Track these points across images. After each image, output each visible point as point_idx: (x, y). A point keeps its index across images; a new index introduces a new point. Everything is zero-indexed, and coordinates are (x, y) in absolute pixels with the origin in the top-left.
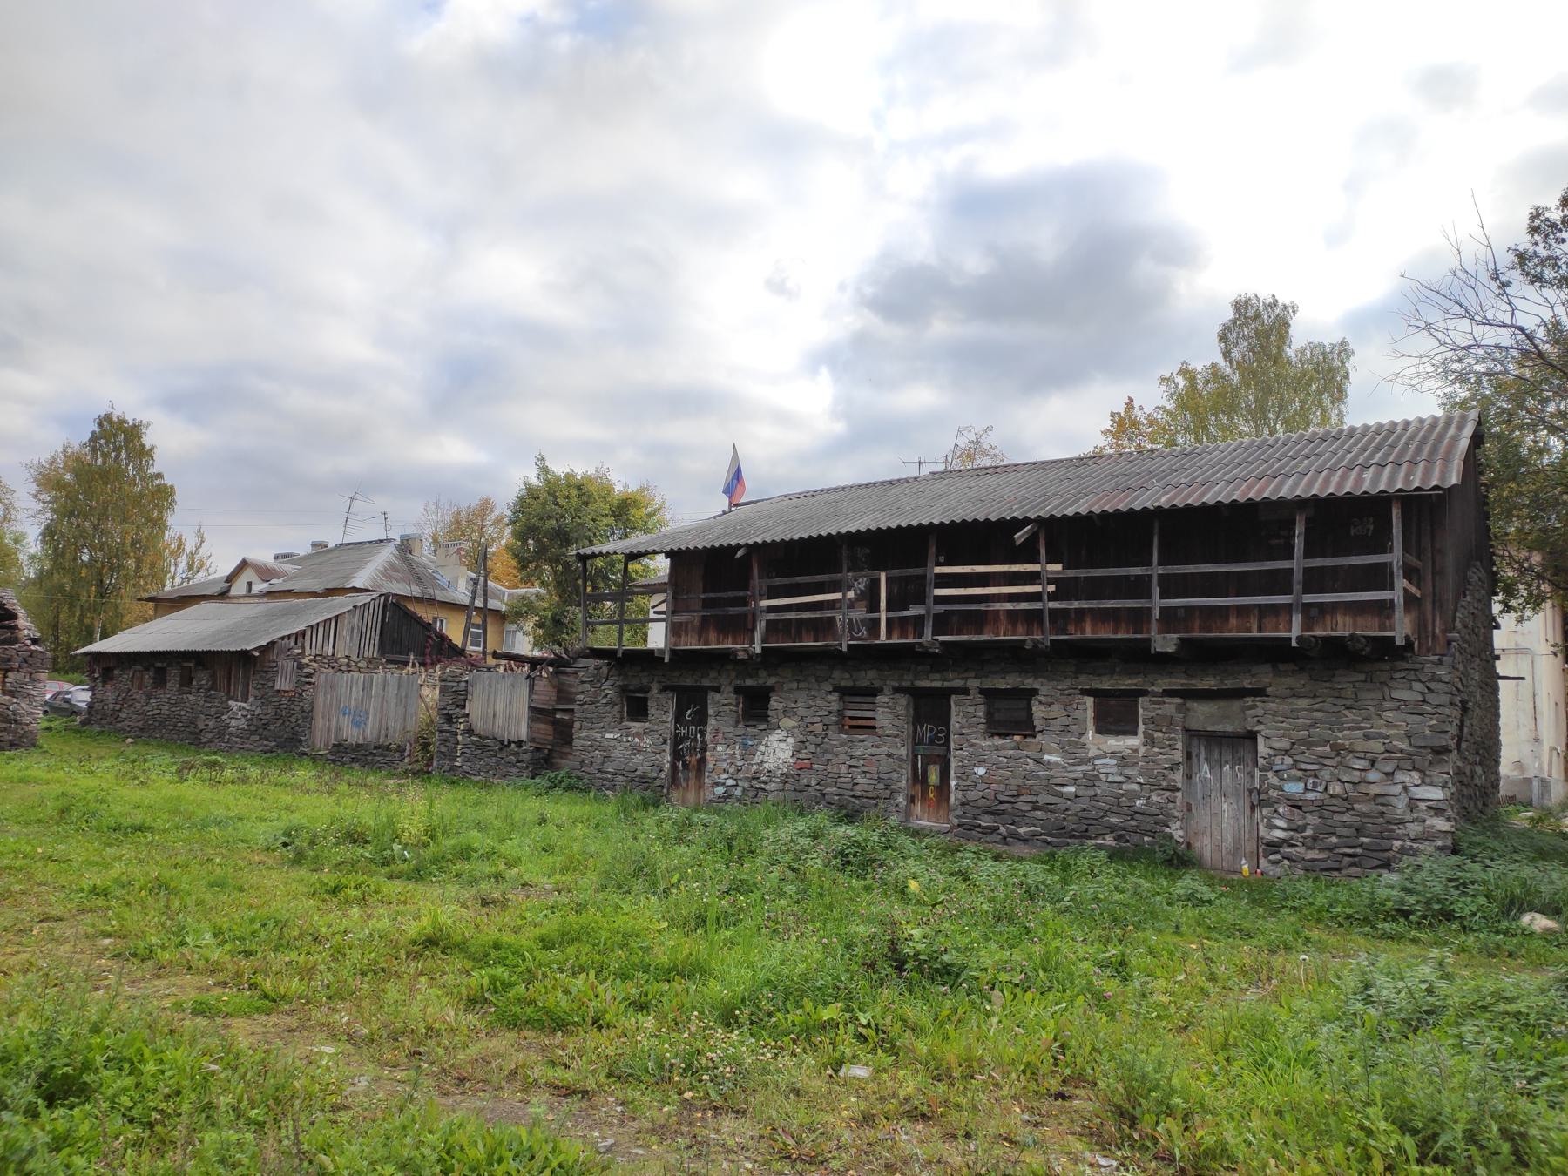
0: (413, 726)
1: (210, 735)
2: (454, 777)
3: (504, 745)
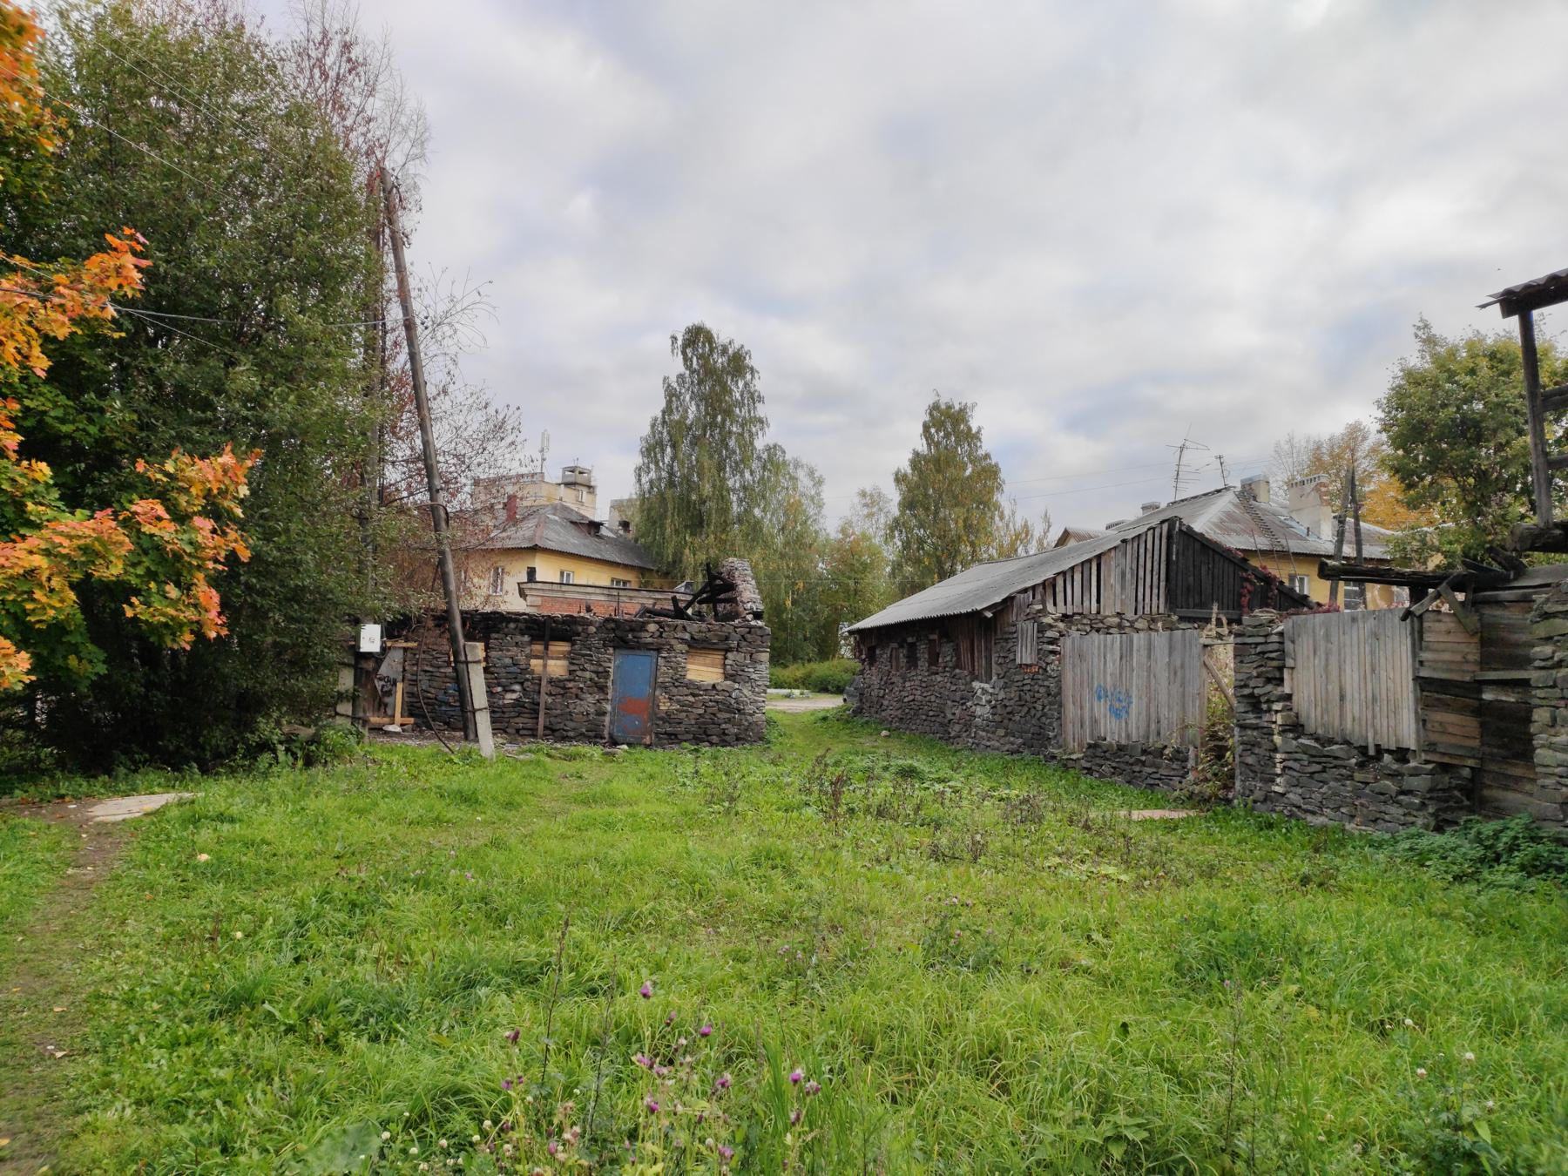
0: (1196, 717)
1: (957, 728)
2: (1269, 817)
3: (1369, 756)
